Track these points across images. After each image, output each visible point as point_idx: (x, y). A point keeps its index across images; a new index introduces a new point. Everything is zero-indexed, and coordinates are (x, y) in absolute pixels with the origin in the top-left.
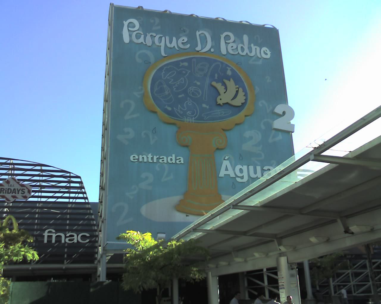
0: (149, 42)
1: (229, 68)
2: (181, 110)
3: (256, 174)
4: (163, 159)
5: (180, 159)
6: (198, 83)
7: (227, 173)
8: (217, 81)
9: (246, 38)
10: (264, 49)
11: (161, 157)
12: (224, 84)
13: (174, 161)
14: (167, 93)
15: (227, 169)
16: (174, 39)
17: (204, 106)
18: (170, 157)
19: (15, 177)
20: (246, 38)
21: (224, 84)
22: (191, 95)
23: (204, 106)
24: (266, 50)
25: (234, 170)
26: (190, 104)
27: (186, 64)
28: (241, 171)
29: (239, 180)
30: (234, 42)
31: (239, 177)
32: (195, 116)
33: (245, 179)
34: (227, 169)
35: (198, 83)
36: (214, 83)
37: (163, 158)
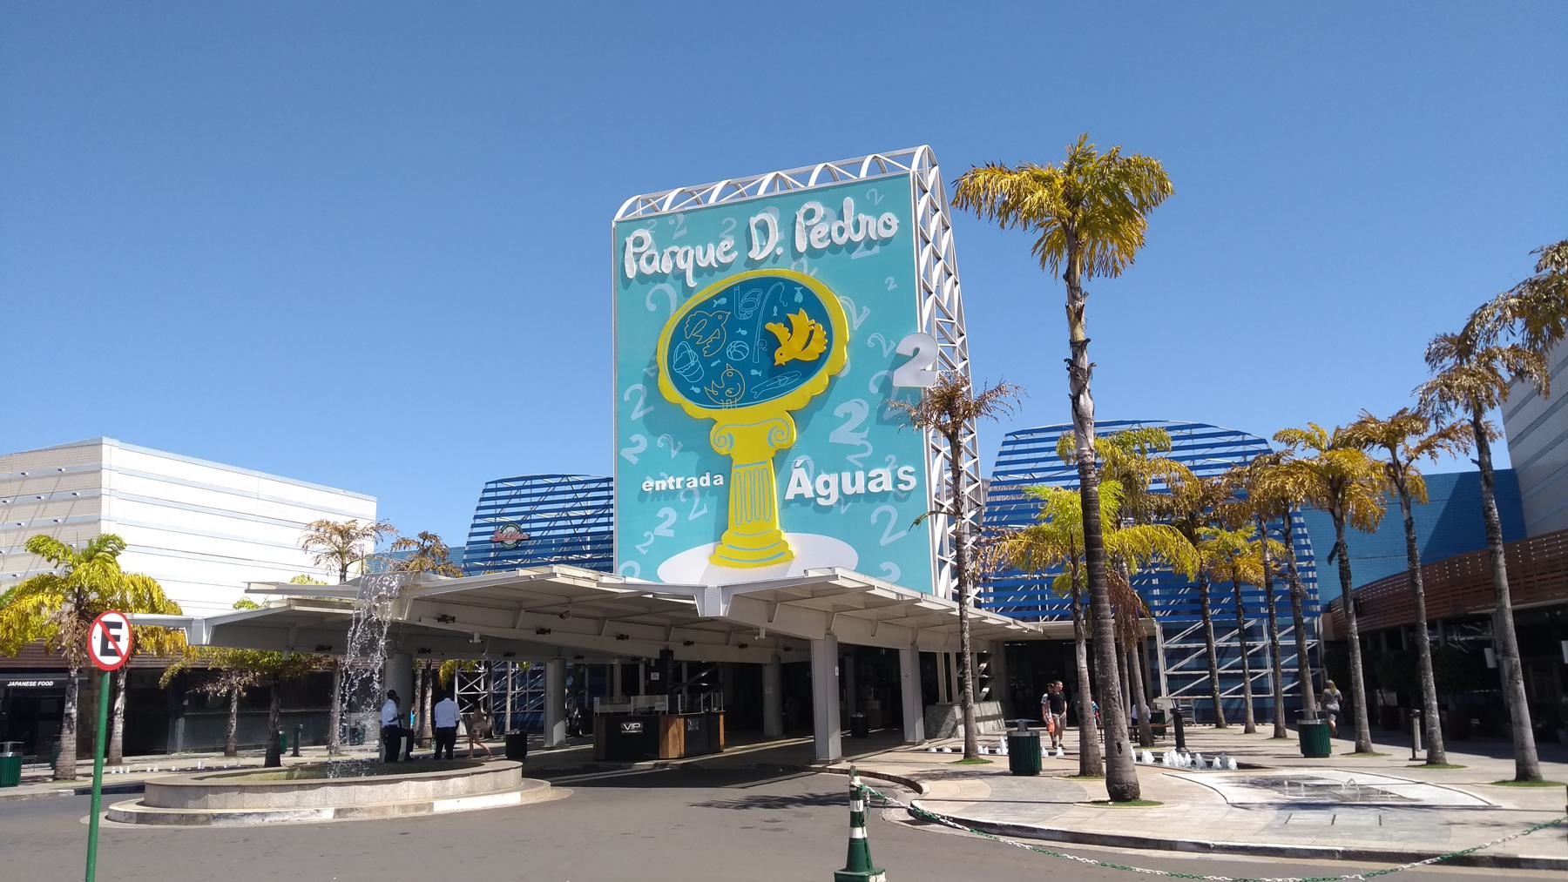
0: (667, 268)
1: (798, 289)
2: (715, 389)
3: (828, 487)
4: (879, 480)
5: (880, 476)
6: (744, 333)
7: (799, 491)
8: (775, 321)
9: (849, 202)
10: (886, 216)
11: (689, 479)
12: (789, 325)
13: (708, 484)
14: (692, 363)
15: (799, 484)
16: (711, 246)
17: (754, 372)
18: (703, 478)
19: (919, 780)
20: (849, 202)
21: (789, 325)
22: (732, 358)
23: (754, 372)
24: (889, 219)
25: (813, 482)
26: (730, 374)
27: (723, 301)
28: (827, 484)
29: (821, 501)
30: (824, 218)
31: (822, 497)
32: (738, 397)
33: (833, 500)
34: (799, 484)
35: (744, 333)
36: (770, 326)
37: (880, 476)
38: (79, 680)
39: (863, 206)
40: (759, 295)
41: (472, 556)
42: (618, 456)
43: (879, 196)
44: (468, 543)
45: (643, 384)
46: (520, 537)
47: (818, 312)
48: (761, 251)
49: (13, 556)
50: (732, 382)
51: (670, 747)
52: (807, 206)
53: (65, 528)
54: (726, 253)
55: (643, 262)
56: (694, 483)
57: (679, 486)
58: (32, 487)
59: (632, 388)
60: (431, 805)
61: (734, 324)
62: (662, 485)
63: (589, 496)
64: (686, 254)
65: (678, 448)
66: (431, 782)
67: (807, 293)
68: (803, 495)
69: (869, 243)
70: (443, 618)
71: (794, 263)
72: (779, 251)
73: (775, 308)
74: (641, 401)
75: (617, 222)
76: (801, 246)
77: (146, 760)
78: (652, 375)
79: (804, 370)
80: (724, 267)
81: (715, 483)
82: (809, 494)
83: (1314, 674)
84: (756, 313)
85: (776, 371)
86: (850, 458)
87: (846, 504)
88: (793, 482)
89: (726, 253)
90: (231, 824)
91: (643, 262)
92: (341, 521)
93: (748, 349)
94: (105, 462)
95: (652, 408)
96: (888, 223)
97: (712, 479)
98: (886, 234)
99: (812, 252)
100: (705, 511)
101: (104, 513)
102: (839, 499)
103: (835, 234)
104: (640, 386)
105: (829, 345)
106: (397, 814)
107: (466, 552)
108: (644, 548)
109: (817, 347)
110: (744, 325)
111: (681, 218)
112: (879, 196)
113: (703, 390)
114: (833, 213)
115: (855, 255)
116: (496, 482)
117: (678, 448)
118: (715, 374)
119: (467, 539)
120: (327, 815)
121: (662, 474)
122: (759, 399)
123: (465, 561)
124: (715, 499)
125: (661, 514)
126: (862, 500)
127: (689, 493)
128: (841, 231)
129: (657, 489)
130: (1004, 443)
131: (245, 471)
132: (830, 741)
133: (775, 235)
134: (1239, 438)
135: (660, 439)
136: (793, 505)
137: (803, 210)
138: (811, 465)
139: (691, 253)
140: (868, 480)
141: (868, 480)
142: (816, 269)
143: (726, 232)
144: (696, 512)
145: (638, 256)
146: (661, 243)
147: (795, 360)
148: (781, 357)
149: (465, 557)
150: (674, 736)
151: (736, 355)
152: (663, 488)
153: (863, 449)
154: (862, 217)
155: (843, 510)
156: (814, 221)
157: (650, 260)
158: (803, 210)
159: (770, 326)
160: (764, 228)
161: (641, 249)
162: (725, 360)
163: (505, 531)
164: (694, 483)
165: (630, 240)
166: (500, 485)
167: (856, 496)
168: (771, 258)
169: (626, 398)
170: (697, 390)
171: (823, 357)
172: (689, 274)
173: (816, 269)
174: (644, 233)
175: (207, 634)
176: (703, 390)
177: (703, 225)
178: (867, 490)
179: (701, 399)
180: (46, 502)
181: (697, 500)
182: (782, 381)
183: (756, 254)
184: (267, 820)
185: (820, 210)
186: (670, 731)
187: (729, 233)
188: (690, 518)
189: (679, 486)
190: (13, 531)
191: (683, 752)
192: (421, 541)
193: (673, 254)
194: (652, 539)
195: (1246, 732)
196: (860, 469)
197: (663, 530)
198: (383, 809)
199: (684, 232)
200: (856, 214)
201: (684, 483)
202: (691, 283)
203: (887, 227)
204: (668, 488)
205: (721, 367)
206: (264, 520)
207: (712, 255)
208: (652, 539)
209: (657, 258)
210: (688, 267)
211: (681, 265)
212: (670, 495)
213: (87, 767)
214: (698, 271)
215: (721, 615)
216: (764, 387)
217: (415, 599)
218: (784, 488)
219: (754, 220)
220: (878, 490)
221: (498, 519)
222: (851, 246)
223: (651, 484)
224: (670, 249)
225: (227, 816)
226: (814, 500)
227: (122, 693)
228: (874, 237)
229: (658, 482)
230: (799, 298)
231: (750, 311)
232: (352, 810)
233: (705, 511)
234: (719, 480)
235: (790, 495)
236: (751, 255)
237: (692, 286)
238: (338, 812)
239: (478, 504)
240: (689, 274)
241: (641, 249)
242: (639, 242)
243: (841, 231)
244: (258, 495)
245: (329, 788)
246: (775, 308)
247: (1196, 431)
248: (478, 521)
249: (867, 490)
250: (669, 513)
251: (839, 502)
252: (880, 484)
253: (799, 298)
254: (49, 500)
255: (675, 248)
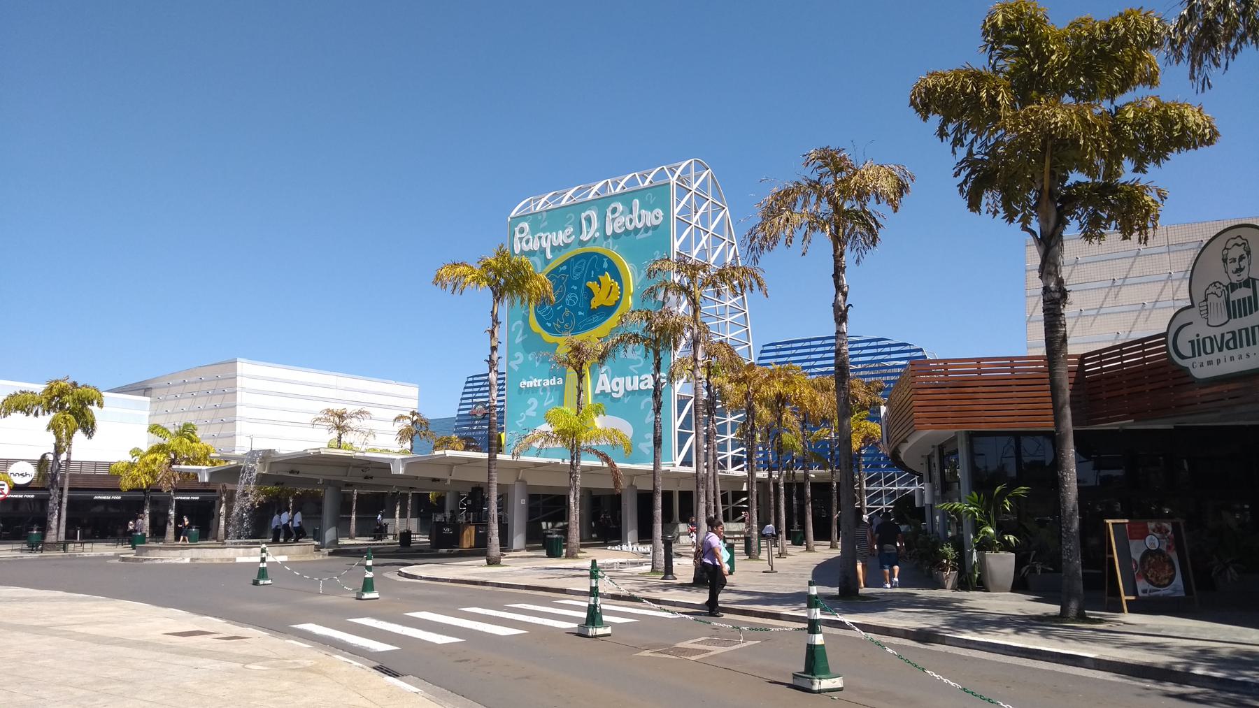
2: (559, 324)
4: (646, 382)
5: (646, 379)
6: (575, 288)
7: (603, 388)
8: (593, 280)
9: (636, 202)
12: (599, 283)
13: (554, 384)
15: (603, 385)
17: (580, 313)
20: (636, 202)
21: (599, 283)
23: (580, 313)
25: (610, 383)
27: (565, 267)
28: (618, 384)
29: (614, 395)
30: (622, 213)
34: (603, 385)
35: (575, 288)
36: (590, 284)
37: (646, 379)
38: (358, 494)
39: (645, 205)
40: (584, 264)
41: (460, 423)
42: (507, 364)
43: (653, 198)
44: (458, 415)
45: (523, 321)
46: (485, 412)
47: (616, 275)
48: (587, 234)
49: (1132, 257)
50: (568, 320)
51: (465, 542)
52: (613, 205)
53: (221, 410)
54: (568, 237)
55: (524, 243)
56: (548, 383)
57: (539, 385)
58: (205, 386)
59: (516, 323)
60: (235, 559)
61: (570, 282)
62: (530, 384)
63: (802, 343)
64: (547, 237)
65: (539, 361)
66: (242, 549)
67: (610, 262)
68: (604, 391)
69: (647, 229)
70: (292, 472)
71: (605, 242)
72: (597, 234)
73: (593, 272)
74: (521, 331)
75: (511, 218)
76: (609, 232)
77: (993, 596)
78: (527, 315)
79: (607, 311)
80: (567, 246)
81: (558, 383)
82: (608, 390)
83: (725, 509)
84: (582, 275)
85: (592, 312)
86: (631, 368)
87: (628, 396)
88: (600, 383)
89: (568, 237)
90: (150, 562)
91: (524, 243)
92: (337, 407)
93: (577, 297)
94: (239, 372)
95: (526, 335)
96: (657, 215)
97: (557, 381)
98: (656, 223)
99: (615, 235)
100: (553, 400)
101: (239, 400)
102: (624, 394)
103: (628, 224)
104: (520, 322)
105: (621, 296)
106: (218, 561)
107: (456, 421)
108: (520, 423)
109: (614, 297)
110: (575, 283)
111: (545, 214)
112: (653, 198)
113: (552, 324)
114: (628, 211)
115: (638, 237)
116: (473, 377)
117: (539, 361)
118: (559, 314)
119: (457, 413)
120: (187, 560)
121: (531, 377)
122: (582, 330)
123: (456, 427)
124: (558, 392)
125: (529, 402)
126: (636, 394)
127: (544, 389)
128: (631, 221)
129: (528, 386)
130: (762, 352)
131: (327, 372)
132: (514, 540)
133: (595, 225)
134: (907, 348)
135: (530, 355)
136: (599, 397)
137: (610, 208)
138: (610, 372)
139: (550, 236)
140: (640, 381)
141: (640, 381)
142: (617, 246)
143: (569, 223)
144: (548, 401)
145: (521, 239)
146: (533, 232)
147: (602, 305)
148: (595, 304)
149: (456, 424)
150: (467, 535)
151: (571, 302)
152: (531, 386)
153: (639, 361)
154: (643, 211)
155: (626, 400)
156: (616, 215)
157: (527, 242)
158: (610, 208)
159: (590, 284)
160: (589, 220)
161: (523, 235)
162: (565, 305)
163: (477, 408)
164: (548, 383)
165: (517, 229)
166: (475, 379)
167: (633, 392)
168: (592, 240)
169: (513, 330)
170: (549, 325)
171: (618, 302)
172: (548, 251)
173: (617, 246)
174: (526, 225)
175: (402, 467)
176: (552, 324)
177: (555, 219)
178: (639, 388)
179: (551, 330)
180: (211, 395)
181: (549, 394)
182: (595, 318)
183: (585, 237)
184: (163, 562)
185: (620, 207)
186: (465, 534)
187: (570, 224)
188: (545, 404)
189: (539, 385)
190: (197, 411)
191: (473, 544)
192: (411, 416)
193: (540, 238)
194: (524, 417)
195: (832, 547)
196: (636, 375)
197: (531, 412)
198: (212, 559)
199: (546, 223)
200: (640, 210)
201: (542, 383)
202: (549, 256)
203: (657, 218)
204: (533, 386)
205: (562, 310)
206: (341, 401)
207: (560, 238)
208: (524, 417)
209: (531, 240)
210: (546, 245)
211: (544, 245)
212: (534, 390)
213: (585, 571)
214: (553, 249)
215: (401, 473)
216: (585, 322)
217: (271, 463)
218: (594, 387)
219: (584, 215)
220: (646, 388)
221: (474, 400)
222: (636, 231)
223: (525, 383)
224: (539, 235)
225: (149, 559)
226: (610, 394)
227: (223, 504)
228: (649, 225)
229: (528, 382)
230: (605, 265)
231: (578, 274)
232: (198, 559)
233: (553, 400)
234: (560, 382)
235: (597, 391)
236: (581, 238)
237: (548, 258)
238: (192, 559)
239: (463, 391)
240: (548, 251)
241: (523, 235)
242: (522, 231)
243: (631, 221)
244: (336, 386)
245: (193, 550)
246: (593, 272)
247: (880, 343)
248: (463, 401)
249: (639, 388)
250: (533, 401)
251: (624, 395)
252: (646, 384)
253: (605, 265)
254: (213, 394)
255: (542, 234)
